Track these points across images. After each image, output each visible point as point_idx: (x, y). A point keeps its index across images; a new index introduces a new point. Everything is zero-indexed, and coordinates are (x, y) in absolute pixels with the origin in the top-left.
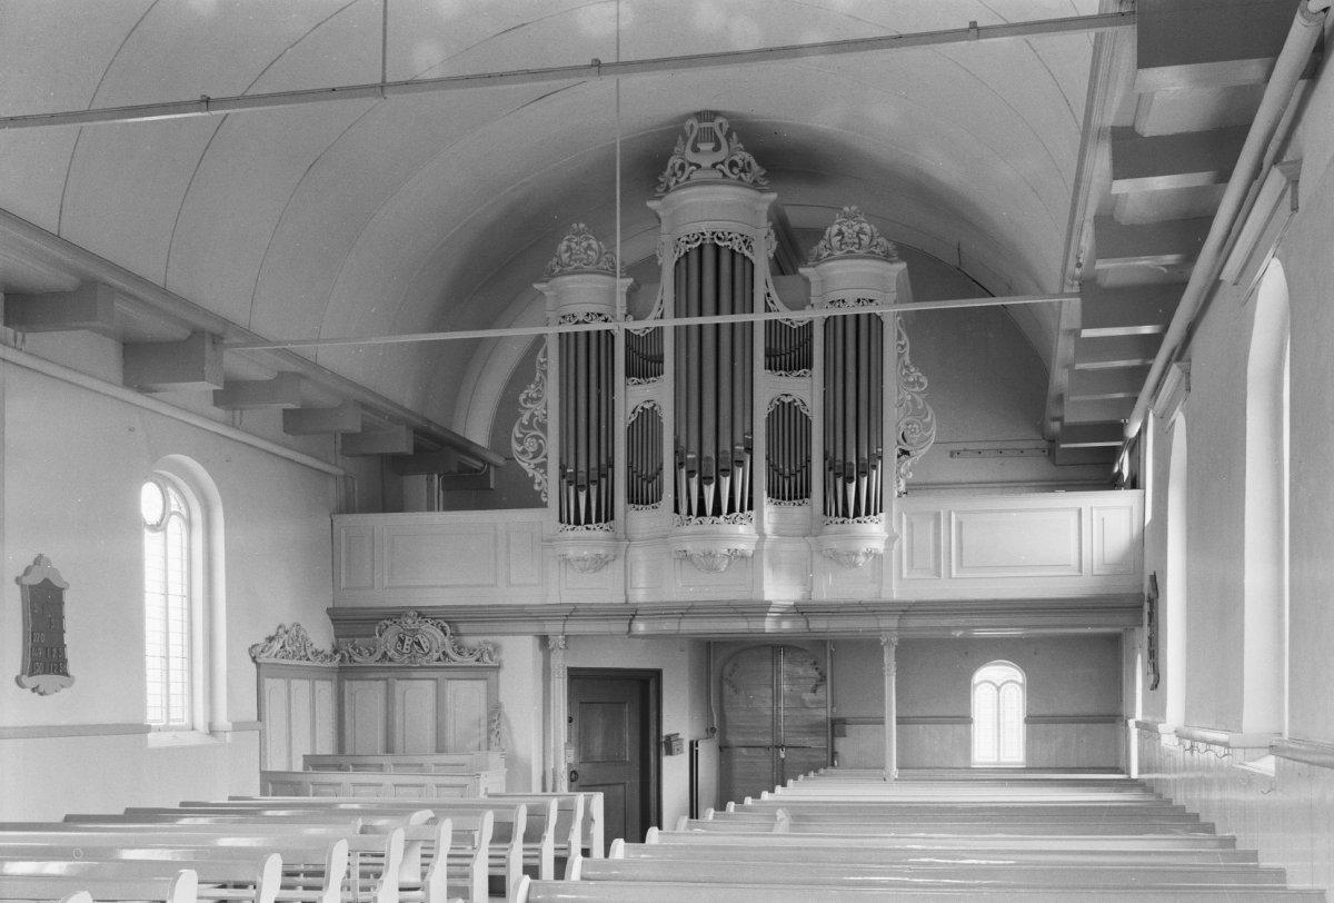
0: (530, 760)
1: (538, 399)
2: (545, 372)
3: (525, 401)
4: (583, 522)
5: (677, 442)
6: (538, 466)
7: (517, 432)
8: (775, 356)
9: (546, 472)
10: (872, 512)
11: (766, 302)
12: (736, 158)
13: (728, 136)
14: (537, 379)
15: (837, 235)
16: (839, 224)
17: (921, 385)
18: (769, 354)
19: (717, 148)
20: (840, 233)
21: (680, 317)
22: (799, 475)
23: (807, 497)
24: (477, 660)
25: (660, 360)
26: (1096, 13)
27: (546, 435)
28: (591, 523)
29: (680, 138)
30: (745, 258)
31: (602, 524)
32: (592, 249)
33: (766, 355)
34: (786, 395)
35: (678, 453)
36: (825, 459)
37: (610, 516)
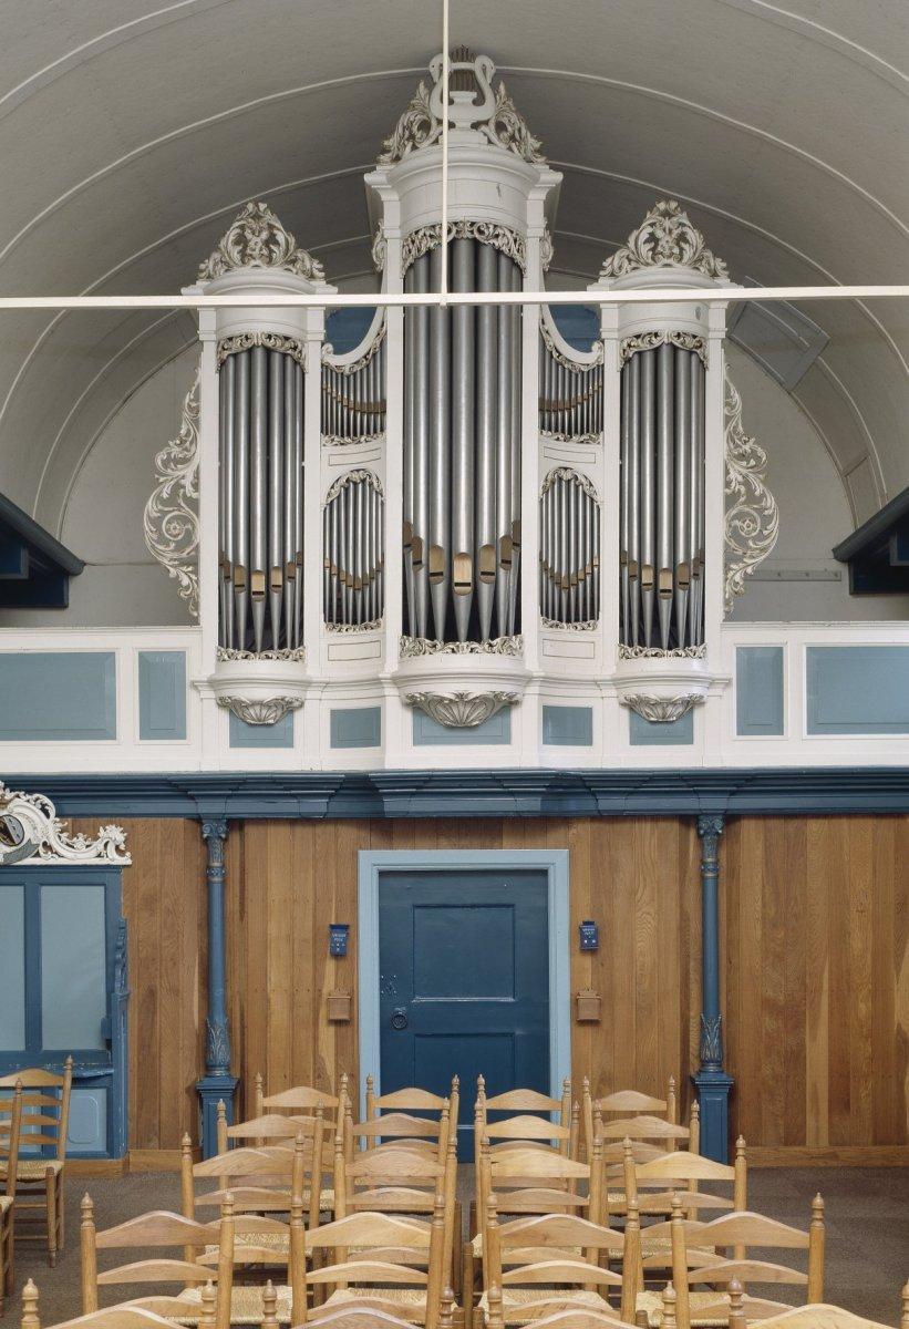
0: (335, 1263)
1: (185, 461)
2: (196, 422)
3: (166, 463)
4: (259, 647)
5: (408, 528)
6: (183, 563)
7: (151, 507)
8: (556, 412)
9: (196, 572)
10: (681, 643)
11: (541, 333)
12: (505, 120)
13: (494, 87)
14: (183, 432)
15: (647, 241)
16: (652, 225)
17: (758, 459)
18: (545, 407)
19: (479, 101)
20: (652, 238)
21: (409, 293)
22: (591, 392)
23: (592, 618)
24: (99, 856)
25: (381, 409)
26: (852, 531)
27: (197, 514)
28: (272, 648)
29: (422, 86)
30: (512, 260)
31: (287, 650)
32: (277, 243)
33: (541, 410)
34: (566, 469)
35: (410, 542)
36: (622, 564)
37: (298, 640)
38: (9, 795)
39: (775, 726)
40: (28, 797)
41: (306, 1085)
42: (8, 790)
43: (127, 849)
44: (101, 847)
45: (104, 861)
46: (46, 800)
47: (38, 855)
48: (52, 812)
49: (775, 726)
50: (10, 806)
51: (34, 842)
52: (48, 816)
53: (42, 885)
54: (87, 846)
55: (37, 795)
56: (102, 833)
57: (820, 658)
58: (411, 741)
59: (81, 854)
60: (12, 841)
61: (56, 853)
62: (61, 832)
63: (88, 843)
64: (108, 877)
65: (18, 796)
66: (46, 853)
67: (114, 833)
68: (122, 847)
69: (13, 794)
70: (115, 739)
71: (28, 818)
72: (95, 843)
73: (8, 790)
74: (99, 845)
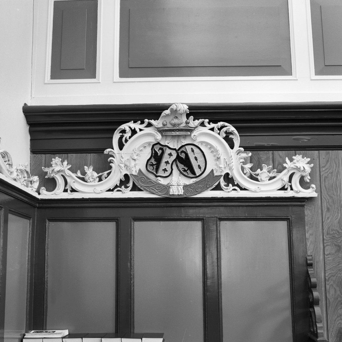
24: (283, 189)
38: (193, 123)
39: (88, 70)
40: (212, 125)
41: (304, 211)
42: (192, 117)
43: (312, 181)
44: (286, 179)
45: (289, 194)
46: (231, 128)
47: (218, 188)
48: (237, 140)
49: (88, 70)
50: (195, 133)
51: (216, 174)
52: (232, 147)
53: (221, 219)
54: (271, 178)
55: (220, 124)
56: (288, 164)
57: (278, 65)
58: (315, 75)
59: (267, 187)
60: (193, 172)
61: (238, 185)
62: (245, 163)
63: (272, 175)
64: (292, 212)
65: (202, 124)
66: (227, 186)
67: (301, 163)
68: (307, 179)
69: (197, 122)
70: (291, 74)
71: (211, 147)
72: (280, 175)
73: (192, 117)
74: (284, 176)
